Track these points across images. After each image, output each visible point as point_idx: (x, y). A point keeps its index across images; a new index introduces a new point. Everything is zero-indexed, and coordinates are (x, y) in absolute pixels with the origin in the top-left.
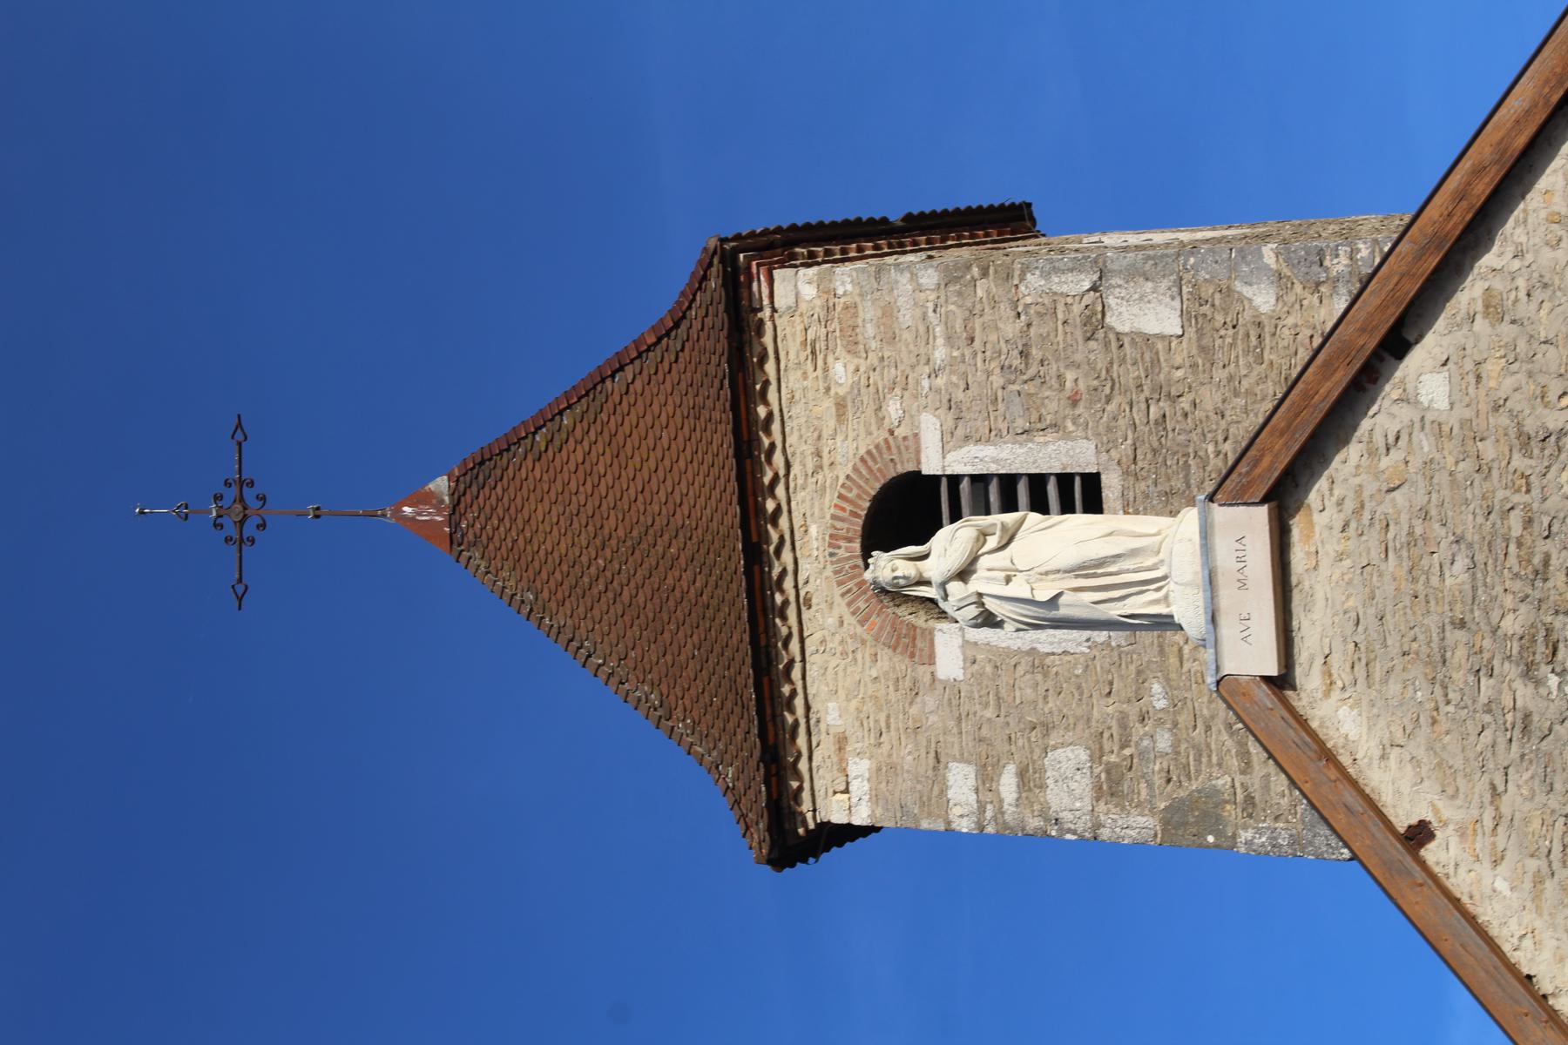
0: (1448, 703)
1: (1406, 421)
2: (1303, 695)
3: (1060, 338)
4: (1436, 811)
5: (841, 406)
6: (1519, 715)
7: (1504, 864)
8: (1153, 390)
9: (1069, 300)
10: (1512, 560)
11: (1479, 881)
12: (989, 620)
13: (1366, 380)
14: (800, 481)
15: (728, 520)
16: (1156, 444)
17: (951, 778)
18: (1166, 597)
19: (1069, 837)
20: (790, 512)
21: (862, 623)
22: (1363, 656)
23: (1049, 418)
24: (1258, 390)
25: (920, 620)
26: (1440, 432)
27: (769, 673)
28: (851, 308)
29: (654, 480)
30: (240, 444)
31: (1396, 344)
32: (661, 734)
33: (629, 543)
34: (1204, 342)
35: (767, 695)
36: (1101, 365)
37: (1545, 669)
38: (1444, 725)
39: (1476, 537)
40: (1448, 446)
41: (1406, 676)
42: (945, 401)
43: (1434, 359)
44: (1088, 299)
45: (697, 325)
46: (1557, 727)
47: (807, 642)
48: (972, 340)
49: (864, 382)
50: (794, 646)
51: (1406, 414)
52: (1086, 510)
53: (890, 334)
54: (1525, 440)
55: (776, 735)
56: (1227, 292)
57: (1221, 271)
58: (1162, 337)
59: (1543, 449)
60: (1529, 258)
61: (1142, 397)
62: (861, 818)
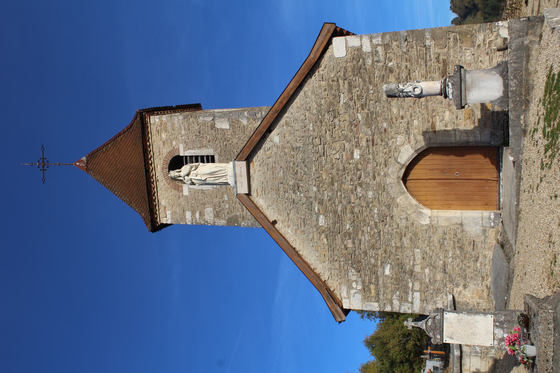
5: (164, 143)
10: (291, 171)
28: (166, 124)
36: (214, 135)
37: (297, 191)
38: (279, 202)
51: (271, 144)
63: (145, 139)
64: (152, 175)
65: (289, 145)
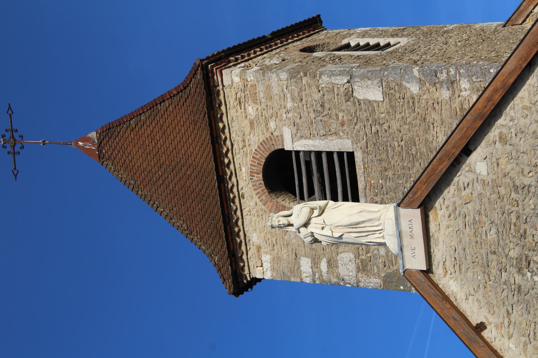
0: (490, 281)
1: (471, 179)
2: (436, 276)
3: (336, 100)
4: (487, 319)
5: (252, 123)
6: (517, 286)
7: (513, 338)
8: (373, 121)
9: (339, 86)
10: (512, 231)
11: (504, 344)
13: (456, 164)
14: (237, 151)
15: (210, 166)
16: (375, 142)
18: (383, 237)
19: (348, 285)
20: (234, 163)
21: (264, 205)
22: (458, 262)
23: (333, 130)
24: (413, 122)
27: (229, 223)
28: (254, 86)
29: (179, 145)
30: (10, 115)
31: (467, 151)
32: (188, 241)
33: (171, 167)
34: (392, 104)
35: (229, 232)
36: (352, 111)
37: (526, 270)
38: (489, 289)
39: (499, 222)
40: (487, 188)
41: (474, 270)
42: (292, 123)
43: (481, 157)
44: (347, 86)
45: (193, 90)
46: (531, 291)
47: (243, 211)
48: (302, 100)
49: (260, 114)
50: (239, 213)
51: (471, 176)
53: (269, 97)
55: (234, 246)
57: (398, 77)
58: (376, 102)
59: (523, 192)
60: (516, 121)
61: (369, 124)
63: (215, 117)
64: (230, 185)
65: (508, 180)
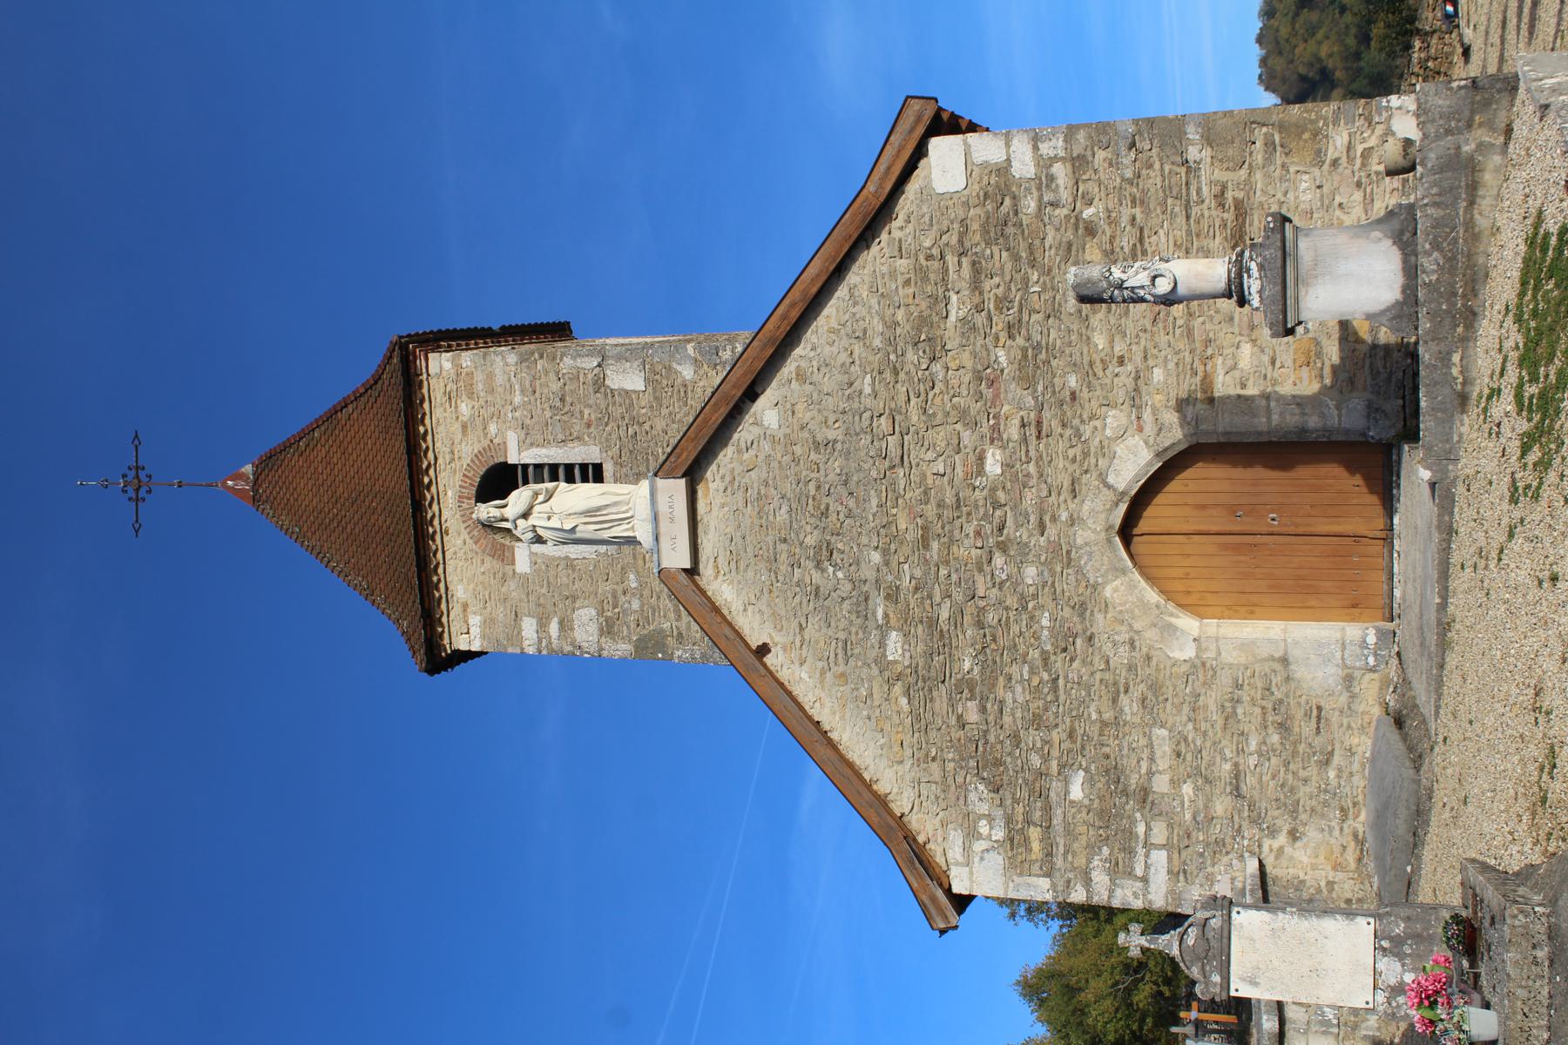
5: (464, 427)
10: (810, 507)
12: (539, 540)
17: (524, 625)
25: (507, 542)
26: (774, 440)
37: (827, 563)
38: (775, 593)
50: (439, 555)
51: (756, 431)
52: (596, 481)
54: (816, 445)
56: (669, 369)
62: (475, 647)
63: (414, 417)
